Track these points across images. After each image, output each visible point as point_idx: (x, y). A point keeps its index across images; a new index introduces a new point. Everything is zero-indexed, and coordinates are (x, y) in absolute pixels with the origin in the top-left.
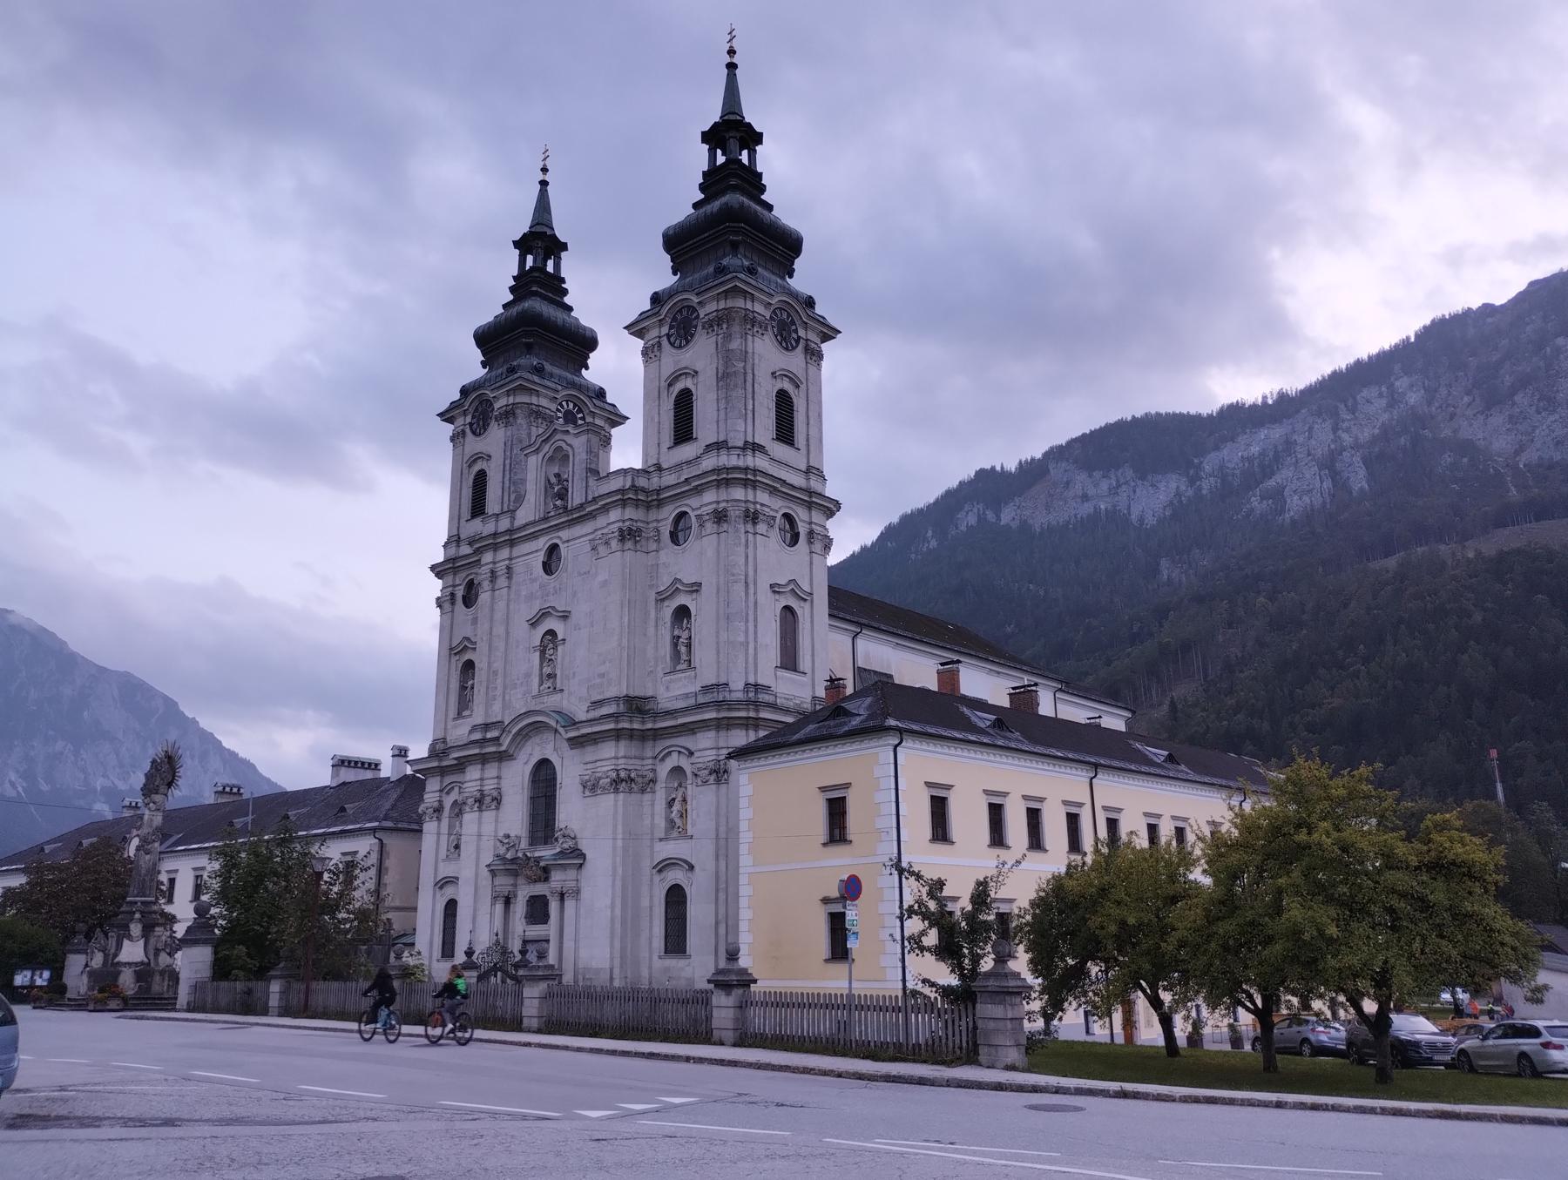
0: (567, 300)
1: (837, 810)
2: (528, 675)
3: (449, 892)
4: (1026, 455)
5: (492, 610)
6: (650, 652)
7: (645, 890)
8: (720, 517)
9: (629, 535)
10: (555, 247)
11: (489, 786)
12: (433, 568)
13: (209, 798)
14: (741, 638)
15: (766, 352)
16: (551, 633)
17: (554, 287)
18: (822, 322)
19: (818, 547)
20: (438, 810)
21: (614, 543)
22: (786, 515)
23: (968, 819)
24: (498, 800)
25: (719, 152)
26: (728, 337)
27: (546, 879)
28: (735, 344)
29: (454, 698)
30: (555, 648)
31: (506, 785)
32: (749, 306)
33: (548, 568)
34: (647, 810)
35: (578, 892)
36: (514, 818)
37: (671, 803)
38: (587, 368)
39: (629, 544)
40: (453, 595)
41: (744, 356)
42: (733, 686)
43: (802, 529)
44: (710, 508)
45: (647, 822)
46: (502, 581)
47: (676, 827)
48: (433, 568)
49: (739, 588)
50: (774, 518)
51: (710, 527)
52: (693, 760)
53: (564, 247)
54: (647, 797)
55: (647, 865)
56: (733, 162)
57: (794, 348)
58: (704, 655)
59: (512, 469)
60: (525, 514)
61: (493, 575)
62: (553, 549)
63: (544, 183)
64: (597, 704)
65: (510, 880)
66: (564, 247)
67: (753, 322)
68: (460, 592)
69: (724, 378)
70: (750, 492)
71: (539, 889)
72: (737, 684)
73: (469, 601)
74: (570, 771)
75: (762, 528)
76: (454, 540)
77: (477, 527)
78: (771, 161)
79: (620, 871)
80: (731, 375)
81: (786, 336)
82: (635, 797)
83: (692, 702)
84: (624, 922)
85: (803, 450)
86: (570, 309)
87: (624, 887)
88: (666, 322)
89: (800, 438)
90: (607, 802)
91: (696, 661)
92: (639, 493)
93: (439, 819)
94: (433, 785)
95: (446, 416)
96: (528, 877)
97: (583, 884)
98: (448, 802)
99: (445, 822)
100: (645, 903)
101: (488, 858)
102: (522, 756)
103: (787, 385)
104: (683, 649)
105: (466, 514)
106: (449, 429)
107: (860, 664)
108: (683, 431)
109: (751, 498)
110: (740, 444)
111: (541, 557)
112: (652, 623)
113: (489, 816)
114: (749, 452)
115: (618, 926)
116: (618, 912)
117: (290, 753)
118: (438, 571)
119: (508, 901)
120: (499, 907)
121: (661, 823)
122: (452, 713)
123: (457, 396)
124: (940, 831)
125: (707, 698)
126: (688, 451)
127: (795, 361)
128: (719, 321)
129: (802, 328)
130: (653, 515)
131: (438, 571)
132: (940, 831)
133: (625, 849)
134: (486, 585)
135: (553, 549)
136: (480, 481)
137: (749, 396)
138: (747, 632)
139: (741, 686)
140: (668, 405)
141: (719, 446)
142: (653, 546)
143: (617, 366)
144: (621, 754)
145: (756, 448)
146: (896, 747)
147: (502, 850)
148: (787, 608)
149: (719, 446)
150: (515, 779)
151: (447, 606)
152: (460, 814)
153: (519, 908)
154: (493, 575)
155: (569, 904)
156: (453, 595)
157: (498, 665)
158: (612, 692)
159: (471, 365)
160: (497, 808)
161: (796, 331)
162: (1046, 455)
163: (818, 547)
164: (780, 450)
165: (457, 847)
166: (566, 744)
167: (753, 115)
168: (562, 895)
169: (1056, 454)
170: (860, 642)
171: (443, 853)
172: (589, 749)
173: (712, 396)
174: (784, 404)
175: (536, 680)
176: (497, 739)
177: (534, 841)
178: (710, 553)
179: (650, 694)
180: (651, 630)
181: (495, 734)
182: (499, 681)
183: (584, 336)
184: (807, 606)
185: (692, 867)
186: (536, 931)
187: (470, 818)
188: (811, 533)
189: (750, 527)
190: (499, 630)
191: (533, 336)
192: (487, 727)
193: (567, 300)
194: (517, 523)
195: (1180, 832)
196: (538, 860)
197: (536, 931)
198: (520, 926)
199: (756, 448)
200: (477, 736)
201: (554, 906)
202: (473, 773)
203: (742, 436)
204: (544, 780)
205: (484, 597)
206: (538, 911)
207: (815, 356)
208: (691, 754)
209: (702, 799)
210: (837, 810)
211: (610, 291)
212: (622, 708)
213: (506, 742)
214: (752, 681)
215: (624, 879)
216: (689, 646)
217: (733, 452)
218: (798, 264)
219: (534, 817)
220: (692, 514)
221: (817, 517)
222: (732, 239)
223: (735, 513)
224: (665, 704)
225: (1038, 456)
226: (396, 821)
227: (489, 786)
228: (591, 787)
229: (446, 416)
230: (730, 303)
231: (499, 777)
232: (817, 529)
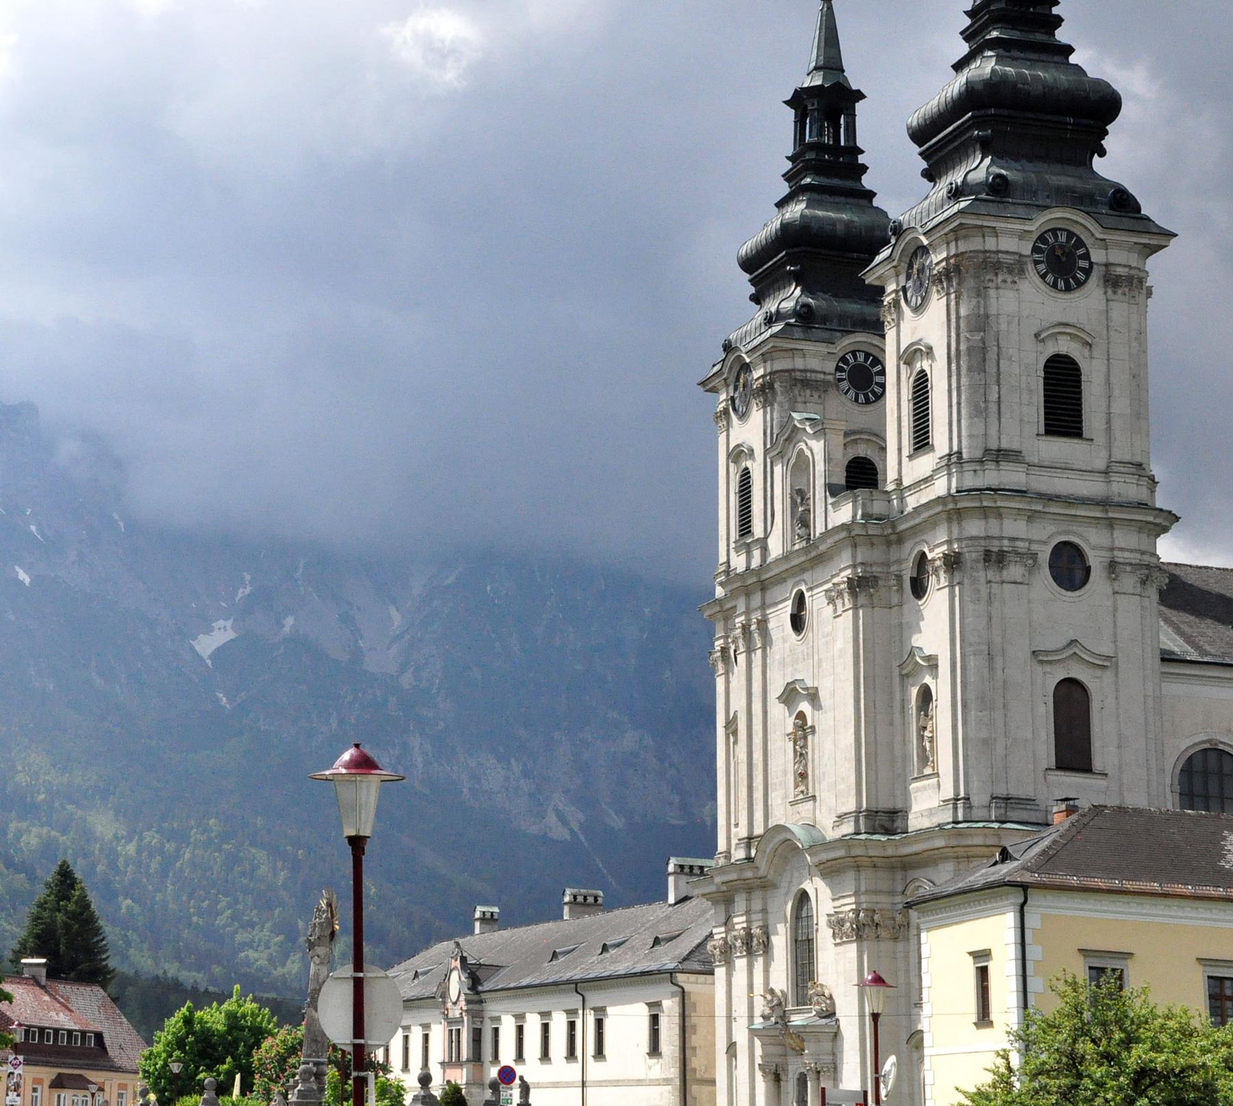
0: (867, 181)
2: (785, 773)
38: (1102, 153)
43: (1095, 560)
53: (859, 96)
54: (900, 946)
57: (1080, 284)
66: (859, 96)
67: (997, 267)
75: (1015, 571)
82: (886, 946)
85: (1100, 439)
86: (871, 195)
103: (1064, 346)
104: (928, 745)
109: (994, 531)
114: (991, 465)
117: (112, 963)
137: (992, 380)
139: (985, 799)
144: (863, 889)
145: (1000, 456)
146: (1022, 906)
161: (1086, 256)
164: (1059, 448)
184: (1108, 676)
188: (1113, 567)
193: (867, 181)
199: (1000, 456)
207: (1128, 284)
217: (967, 467)
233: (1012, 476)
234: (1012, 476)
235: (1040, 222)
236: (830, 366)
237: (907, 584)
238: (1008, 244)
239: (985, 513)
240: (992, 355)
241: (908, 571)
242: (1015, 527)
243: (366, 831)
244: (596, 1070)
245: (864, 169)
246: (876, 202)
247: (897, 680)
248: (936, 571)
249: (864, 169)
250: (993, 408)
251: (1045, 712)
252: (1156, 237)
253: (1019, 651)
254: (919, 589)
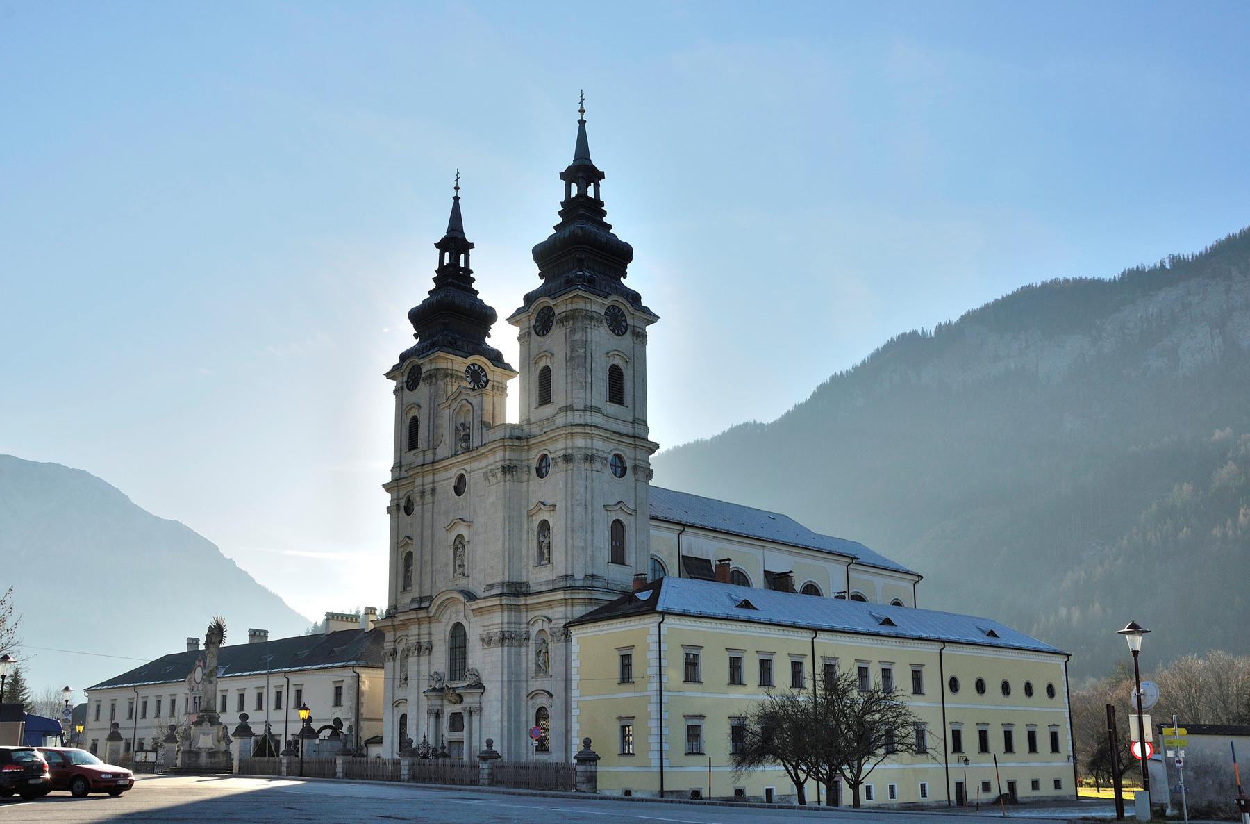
0: (474, 286)
1: (626, 662)
2: (447, 565)
3: (402, 709)
4: (943, 320)
5: (423, 519)
6: (524, 552)
7: (523, 710)
8: (568, 459)
9: (508, 469)
10: (595, 176)
11: (424, 639)
12: (384, 486)
13: (246, 641)
14: (582, 544)
15: (601, 337)
16: (460, 536)
17: (594, 209)
18: (646, 310)
19: (641, 475)
20: (394, 653)
21: (499, 475)
22: (617, 455)
23: (714, 667)
24: (430, 649)
25: (447, 254)
26: (573, 331)
27: (461, 702)
28: (578, 336)
29: (401, 579)
30: (463, 547)
31: (433, 638)
32: (588, 307)
33: (459, 490)
34: (524, 658)
35: (481, 709)
36: (440, 661)
37: (538, 654)
39: (508, 477)
40: (398, 506)
41: (585, 344)
42: (577, 576)
44: (562, 453)
45: (524, 665)
46: (428, 497)
47: (541, 669)
48: (384, 486)
49: (580, 510)
50: (606, 459)
51: (561, 464)
52: (551, 625)
53: (472, 246)
55: (523, 693)
56: (582, 194)
58: (558, 555)
59: (434, 417)
60: (442, 451)
61: (423, 493)
62: (461, 479)
63: (456, 199)
64: (491, 586)
65: (438, 702)
66: (472, 246)
67: (592, 318)
68: (402, 505)
69: (570, 360)
70: (588, 441)
71: (457, 708)
72: (579, 575)
73: (408, 510)
74: (475, 631)
75: (597, 465)
76: (398, 466)
77: (410, 457)
78: (609, 193)
79: (506, 698)
80: (579, 358)
81: (617, 323)
83: (551, 587)
84: (509, 730)
85: (631, 407)
87: (509, 708)
88: (538, 317)
89: (628, 398)
90: (497, 652)
91: (553, 560)
92: (518, 437)
93: (394, 660)
94: (389, 636)
95: (390, 375)
96: (450, 701)
97: (483, 705)
98: (400, 648)
99: (398, 662)
100: (523, 718)
101: (424, 687)
102: (444, 619)
103: (618, 361)
105: (405, 448)
106: (392, 384)
107: (684, 553)
108: (545, 396)
109: (589, 445)
110: (582, 407)
111: (453, 482)
112: (525, 531)
113: (424, 659)
115: (505, 732)
116: (505, 724)
118: (387, 487)
119: (438, 715)
120: (432, 720)
121: (532, 666)
122: (400, 588)
123: (397, 361)
124: (918, 689)
125: (562, 584)
126: (547, 410)
127: (626, 341)
128: (570, 317)
129: (630, 318)
130: (524, 456)
131: (387, 487)
132: (918, 689)
133: (509, 681)
134: (418, 499)
135: (461, 479)
136: (414, 424)
138: (586, 539)
139: (582, 576)
140: (535, 378)
141: (569, 408)
142: (525, 478)
143: (504, 338)
145: (592, 409)
147: (433, 684)
148: (617, 521)
149: (569, 408)
150: (440, 634)
151: (394, 512)
152: (407, 657)
153: (445, 720)
154: (423, 493)
155: (475, 718)
156: (398, 506)
157: (427, 557)
158: (499, 579)
159: (407, 338)
160: (430, 654)
161: (486, 376)
162: (963, 318)
163: (641, 475)
164: (612, 408)
165: (406, 679)
166: (471, 613)
167: (597, 160)
168: (471, 712)
169: (970, 318)
170: (684, 537)
171: (397, 683)
172: (487, 617)
173: (563, 373)
174: (615, 376)
175: (452, 569)
176: (427, 608)
177: (452, 679)
178: (561, 485)
179: (524, 580)
180: (525, 537)
181: (427, 604)
182: (429, 568)
183: (489, 312)
185: (551, 695)
186: (456, 736)
187: (412, 660)
188: (635, 467)
189: (588, 466)
190: (428, 533)
191: (451, 315)
192: (421, 599)
193: (474, 286)
194: (438, 458)
195: (886, 674)
196: (454, 689)
197: (456, 736)
198: (447, 734)
199: (592, 409)
200: (416, 606)
201: (466, 719)
202: (413, 630)
203: (582, 402)
204: (458, 633)
205: (417, 509)
206: (456, 722)
207: (641, 337)
208: (550, 621)
209: (556, 649)
210: (626, 662)
211: (505, 280)
212: (505, 591)
213: (433, 609)
214: (590, 573)
215: (509, 702)
216: (549, 548)
218: (630, 268)
219: (452, 660)
220: (550, 456)
221: (640, 454)
222: (584, 255)
223: (578, 456)
224: (534, 588)
225: (955, 319)
226: (573, 546)
227: (424, 639)
228: (487, 641)
229: (390, 375)
230: (575, 306)
231: (430, 634)
232: (640, 463)
233: (597, 419)
234: (597, 419)
235: (608, 302)
236: (464, 369)
237: (534, 471)
238: (596, 308)
239: (585, 435)
240: (589, 360)
241: (534, 464)
242: (598, 444)
243: (1138, 648)
244: (141, 723)
245: (473, 280)
246: (479, 296)
247: (525, 518)
248: (556, 464)
249: (473, 280)
250: (589, 385)
251: (607, 534)
252: (652, 318)
253: (599, 506)
254: (541, 473)
